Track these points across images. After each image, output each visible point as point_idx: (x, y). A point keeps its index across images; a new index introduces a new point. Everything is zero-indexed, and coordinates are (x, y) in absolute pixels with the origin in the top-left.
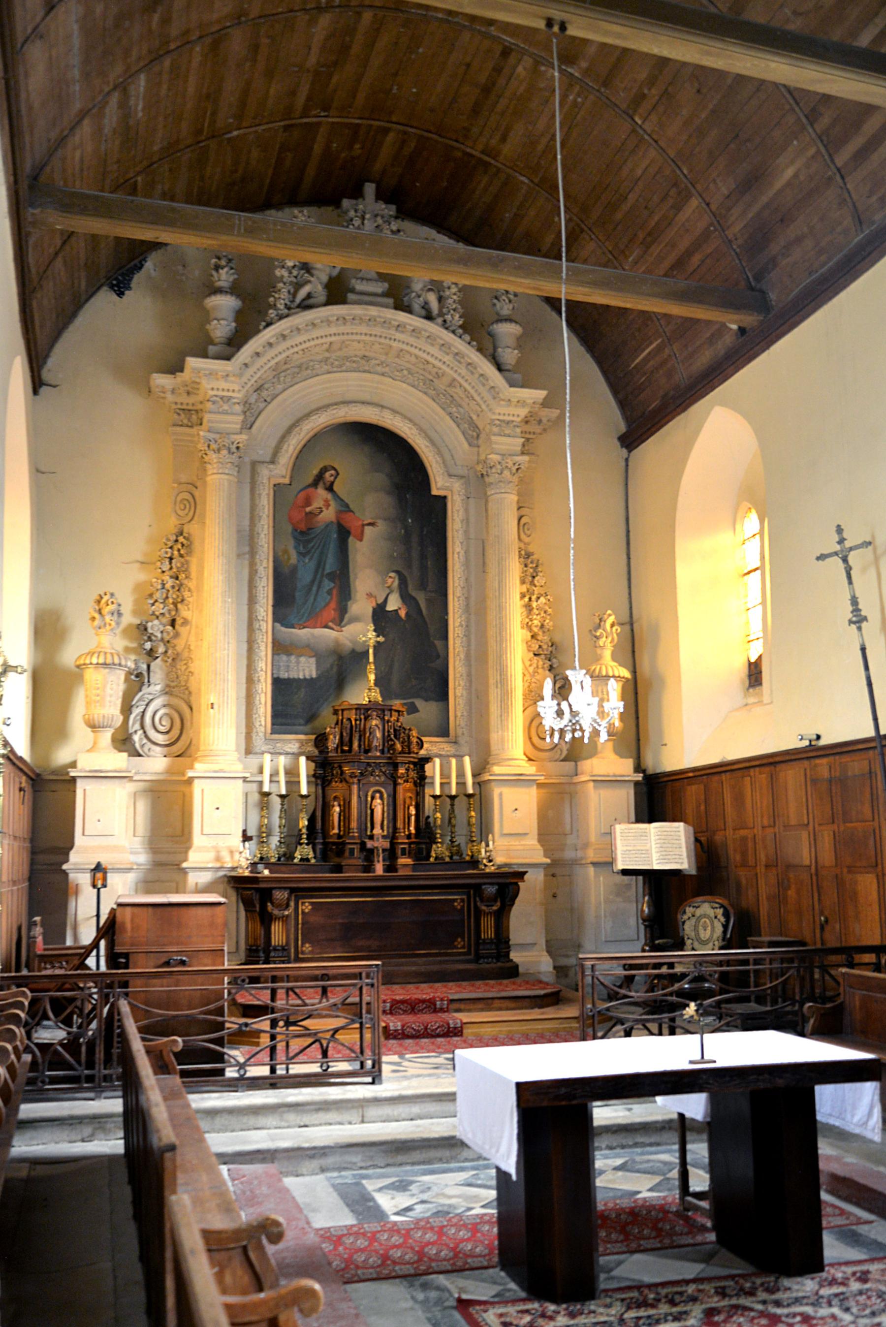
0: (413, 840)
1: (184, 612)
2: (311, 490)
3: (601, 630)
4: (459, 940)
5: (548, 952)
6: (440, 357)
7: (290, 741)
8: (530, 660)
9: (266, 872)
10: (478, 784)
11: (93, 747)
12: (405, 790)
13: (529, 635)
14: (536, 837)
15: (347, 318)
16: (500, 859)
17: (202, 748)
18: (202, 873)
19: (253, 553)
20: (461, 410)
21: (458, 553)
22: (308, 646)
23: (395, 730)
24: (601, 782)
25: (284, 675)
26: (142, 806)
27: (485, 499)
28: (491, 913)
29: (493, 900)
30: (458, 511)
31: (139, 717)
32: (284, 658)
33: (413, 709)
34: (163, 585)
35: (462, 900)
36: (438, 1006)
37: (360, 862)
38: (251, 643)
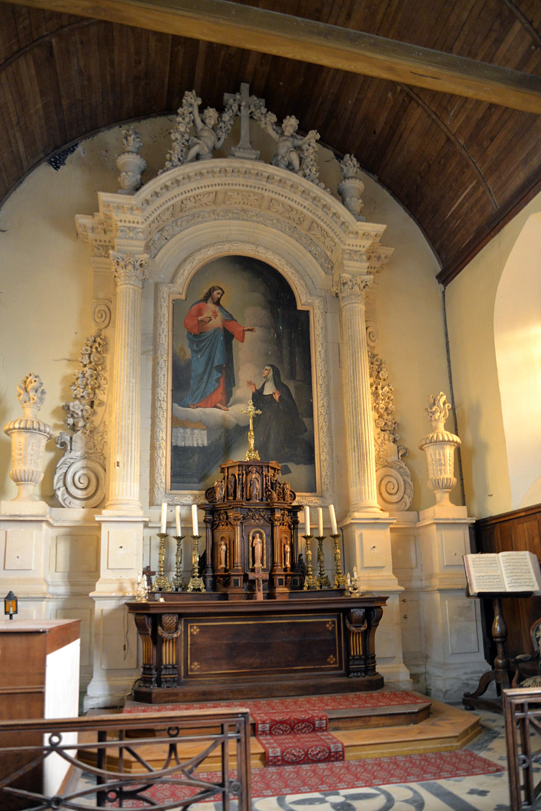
0: (289, 573)
1: (101, 396)
2: (202, 304)
3: (436, 407)
4: (332, 656)
5: (404, 663)
6: (301, 202)
7: (185, 495)
8: (378, 434)
9: (162, 600)
10: (340, 529)
11: (17, 497)
12: (281, 532)
13: (377, 416)
14: (391, 570)
15: (228, 169)
16: (363, 588)
17: (110, 499)
18: (107, 602)
19: (155, 350)
20: (318, 248)
21: (320, 352)
22: (201, 421)
23: (272, 483)
24: (442, 525)
25: (181, 444)
26: (63, 548)
27: (339, 311)
28: (359, 633)
29: (360, 622)
30: (319, 321)
31: (62, 477)
32: (181, 430)
33: (286, 471)
34: (83, 374)
35: (333, 622)
36: (317, 725)
37: (244, 591)
38: (154, 418)
